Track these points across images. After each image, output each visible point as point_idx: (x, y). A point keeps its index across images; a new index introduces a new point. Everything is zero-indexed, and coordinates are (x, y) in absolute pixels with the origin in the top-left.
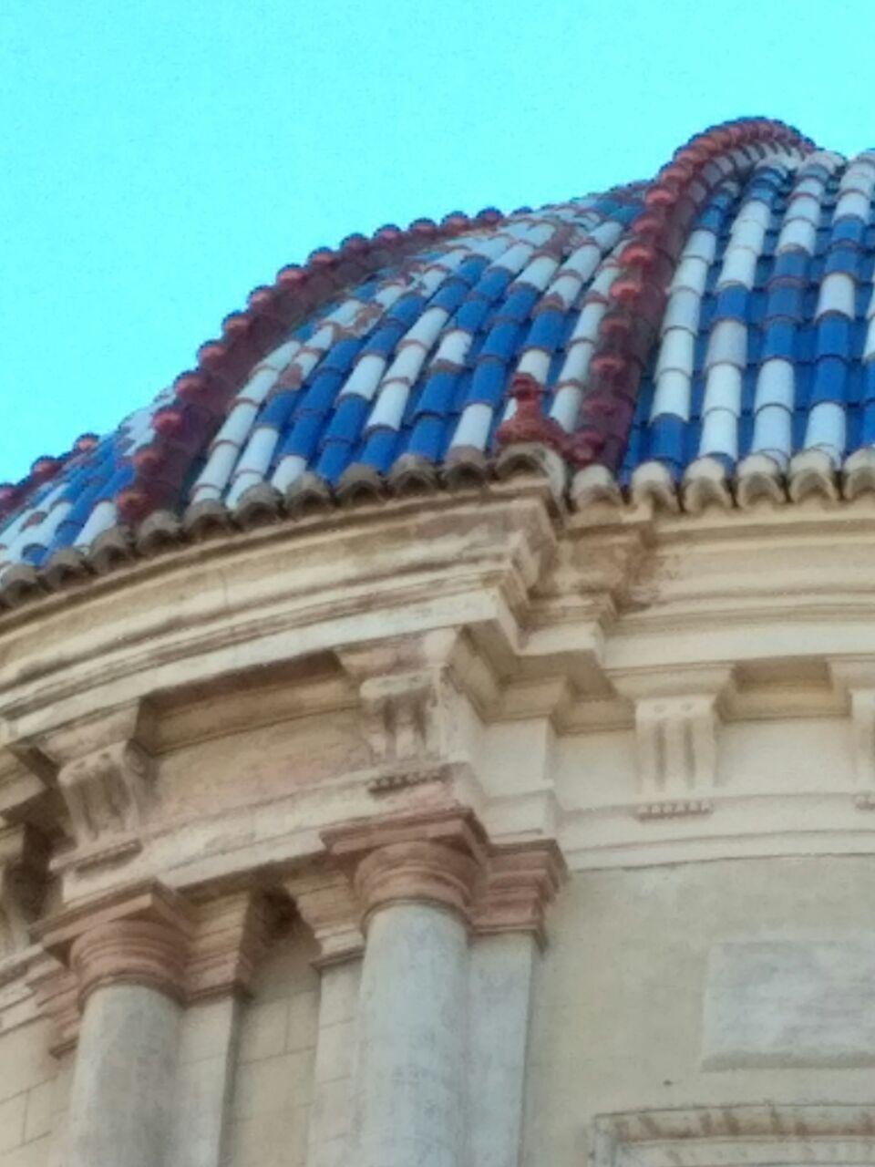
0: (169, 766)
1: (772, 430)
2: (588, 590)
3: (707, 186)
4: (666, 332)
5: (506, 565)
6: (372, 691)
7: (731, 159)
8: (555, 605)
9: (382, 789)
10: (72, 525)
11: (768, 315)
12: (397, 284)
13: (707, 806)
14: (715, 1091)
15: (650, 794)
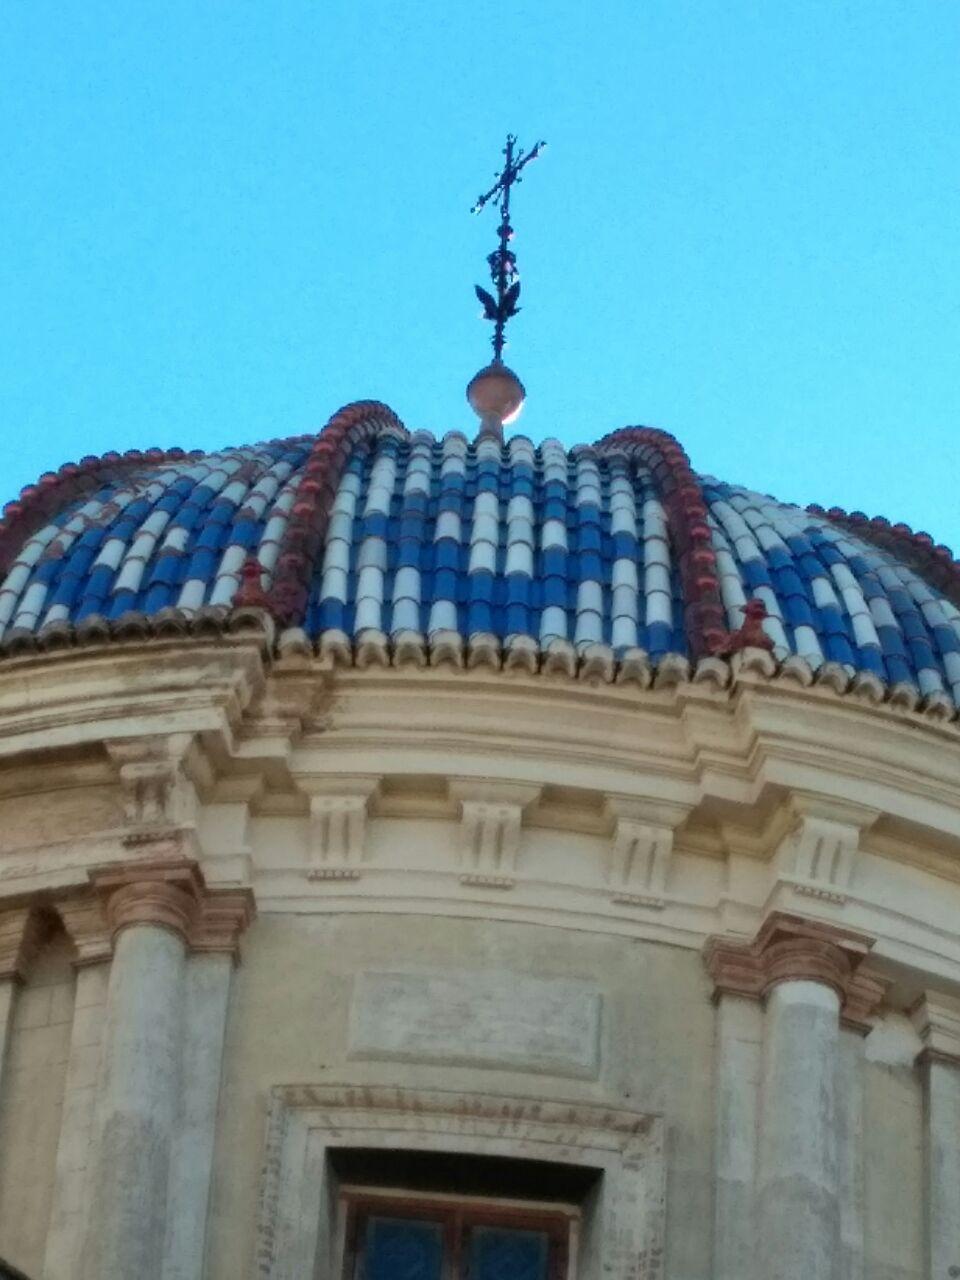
2: (283, 715)
3: (351, 442)
4: (331, 540)
5: (230, 692)
6: (129, 772)
7: (364, 426)
8: (261, 723)
9: (131, 843)
11: (402, 535)
12: (128, 492)
13: (357, 875)
14: (360, 1075)
15: (317, 863)
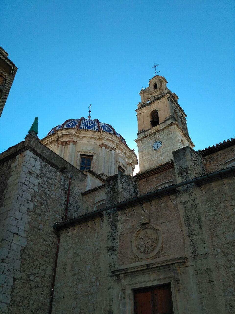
0: (63, 137)
1: (85, 128)
9: (71, 139)
10: (59, 128)
14: (82, 150)
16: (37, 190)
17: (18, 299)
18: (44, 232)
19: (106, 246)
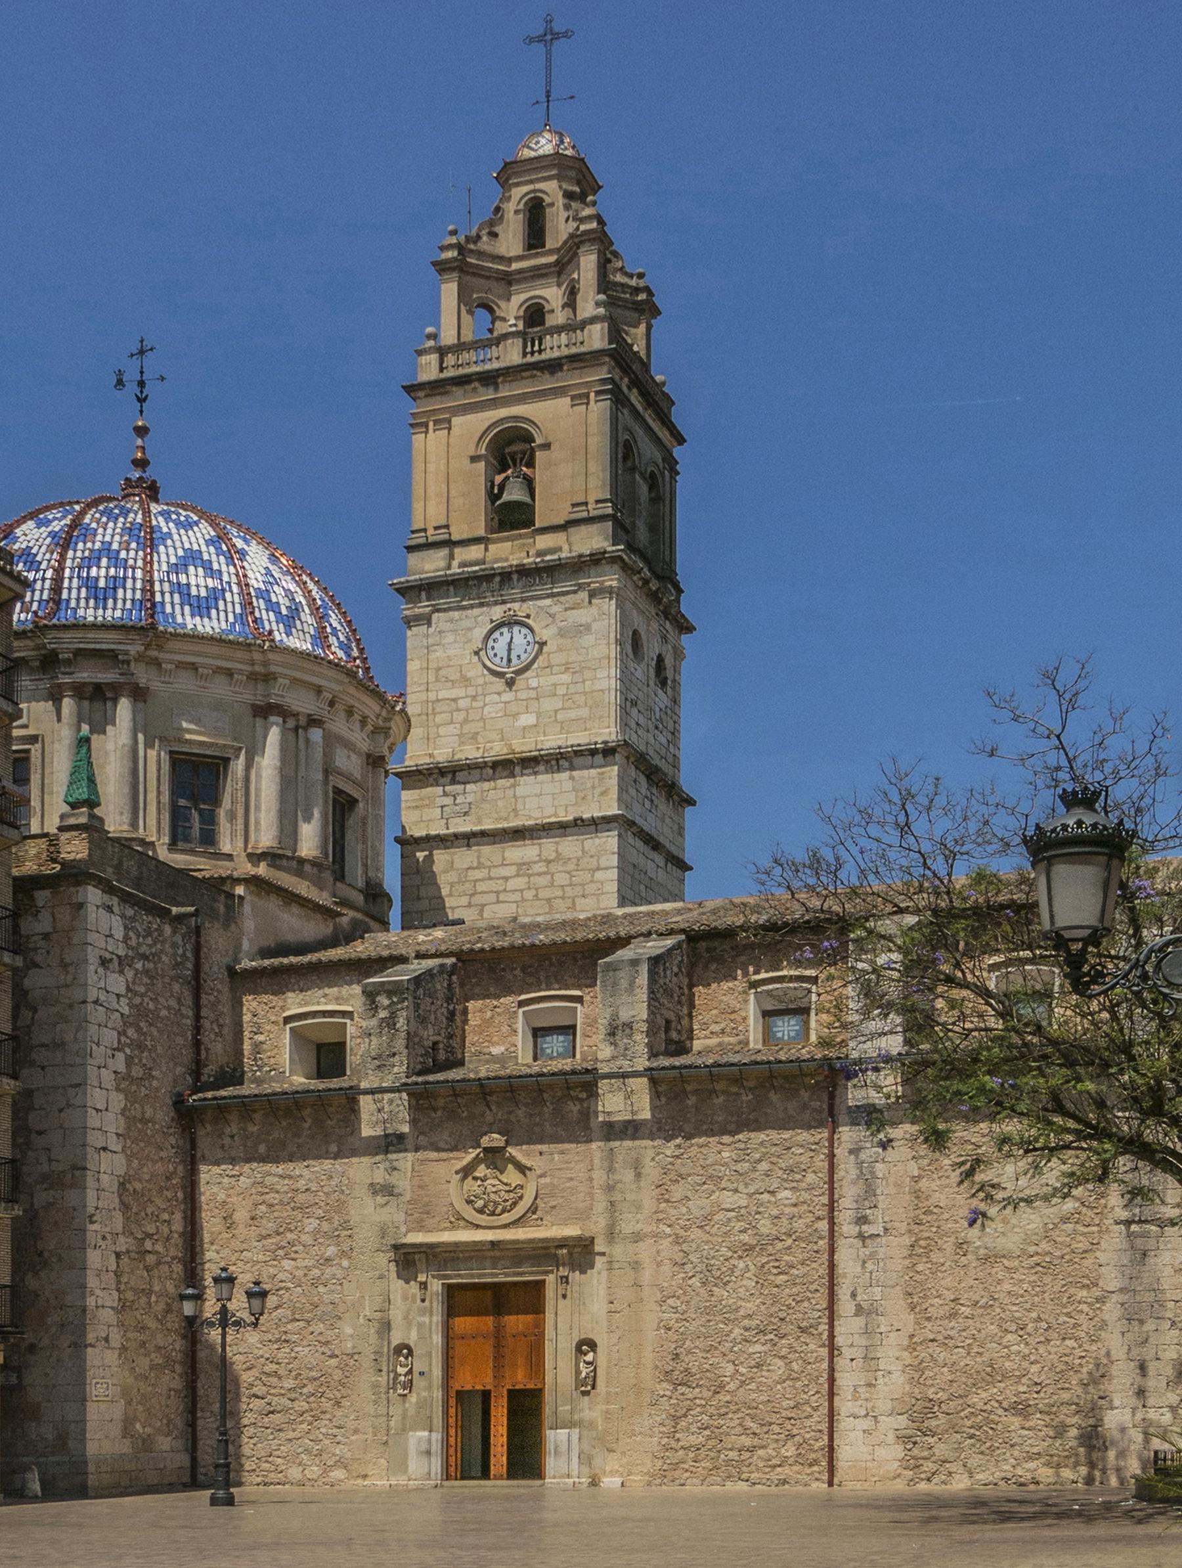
16: (126, 1011)
17: (129, 1295)
18: (157, 1126)
19: (369, 1181)
